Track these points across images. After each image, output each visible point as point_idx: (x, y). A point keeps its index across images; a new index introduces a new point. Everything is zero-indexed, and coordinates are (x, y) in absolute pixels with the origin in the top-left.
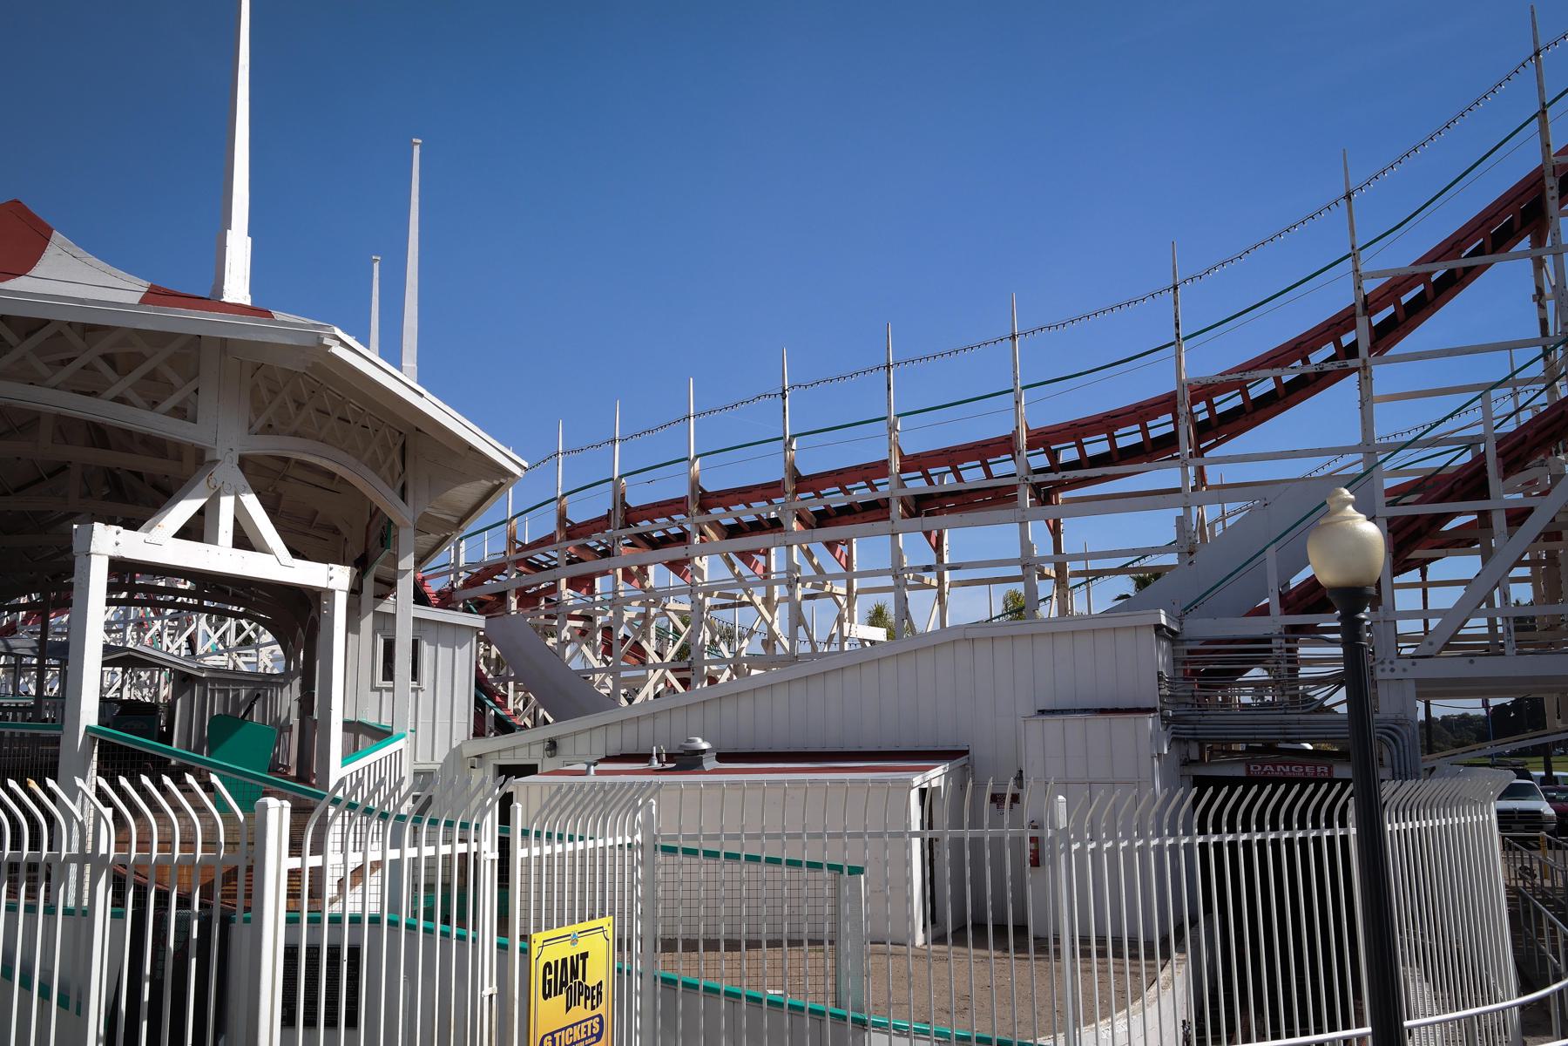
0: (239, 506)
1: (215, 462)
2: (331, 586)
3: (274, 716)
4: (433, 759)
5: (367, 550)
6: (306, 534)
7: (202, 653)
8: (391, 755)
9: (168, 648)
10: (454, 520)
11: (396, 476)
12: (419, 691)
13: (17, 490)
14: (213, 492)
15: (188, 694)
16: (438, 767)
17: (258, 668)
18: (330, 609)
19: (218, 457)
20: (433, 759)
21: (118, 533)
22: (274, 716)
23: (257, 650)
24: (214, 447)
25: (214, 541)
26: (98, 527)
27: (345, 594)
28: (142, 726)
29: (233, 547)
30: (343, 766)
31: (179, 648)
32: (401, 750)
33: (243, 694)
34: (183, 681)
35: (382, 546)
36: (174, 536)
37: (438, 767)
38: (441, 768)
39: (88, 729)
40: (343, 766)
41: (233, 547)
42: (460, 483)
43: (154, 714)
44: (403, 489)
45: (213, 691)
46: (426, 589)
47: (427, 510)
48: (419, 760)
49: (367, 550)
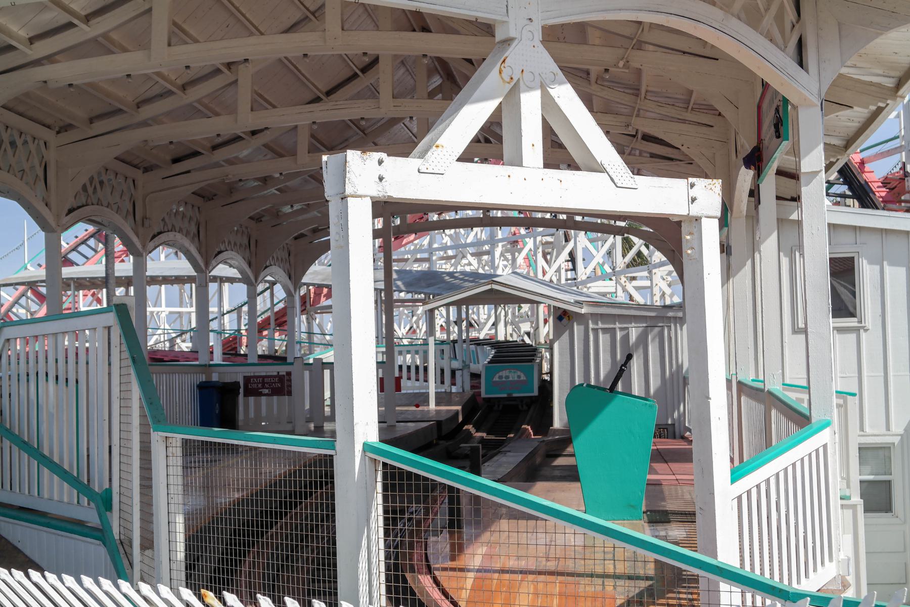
0: (548, 103)
1: (508, 41)
2: (695, 210)
3: (674, 362)
4: (888, 429)
5: (760, 140)
6: (684, 121)
7: (584, 278)
8: (802, 460)
9: (544, 273)
10: (889, 83)
11: (788, 26)
12: (862, 331)
13: (329, 93)
14: (508, 87)
15: (566, 336)
16: (896, 440)
17: (652, 295)
18: (696, 247)
19: (512, 34)
20: (888, 429)
21: (380, 162)
22: (674, 362)
23: (650, 272)
24: (505, 19)
25: (518, 162)
26: (353, 156)
27: (716, 221)
28: (519, 377)
29: (547, 165)
30: (733, 481)
31: (558, 270)
32: (825, 446)
33: (634, 334)
34: (563, 317)
35: (778, 137)
36: (459, 160)
37: (896, 440)
38: (902, 441)
39: (367, 447)
40: (733, 481)
41: (547, 165)
42: (888, 28)
43: (531, 361)
44: (800, 45)
45: (596, 331)
46: (867, 177)
47: (844, 71)
48: (868, 430)
49: (760, 140)
